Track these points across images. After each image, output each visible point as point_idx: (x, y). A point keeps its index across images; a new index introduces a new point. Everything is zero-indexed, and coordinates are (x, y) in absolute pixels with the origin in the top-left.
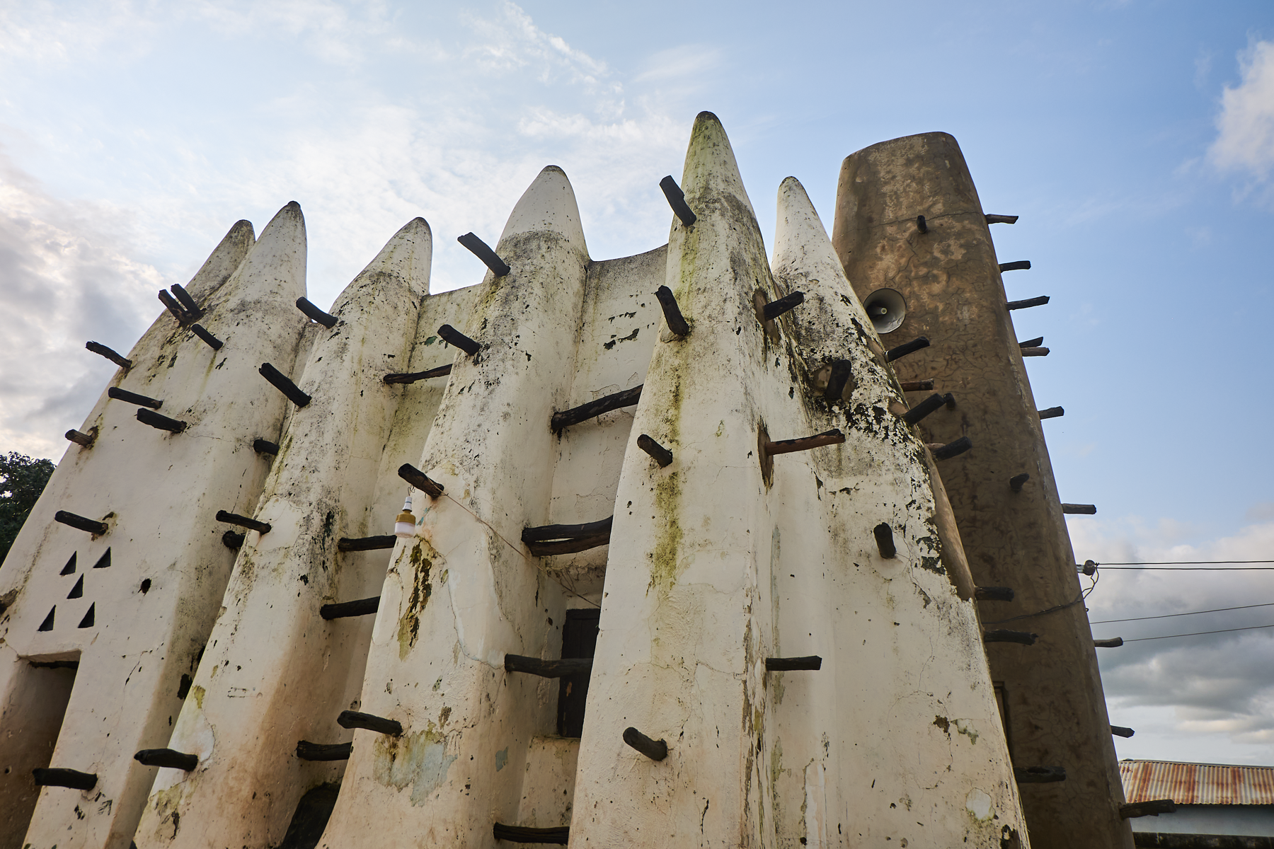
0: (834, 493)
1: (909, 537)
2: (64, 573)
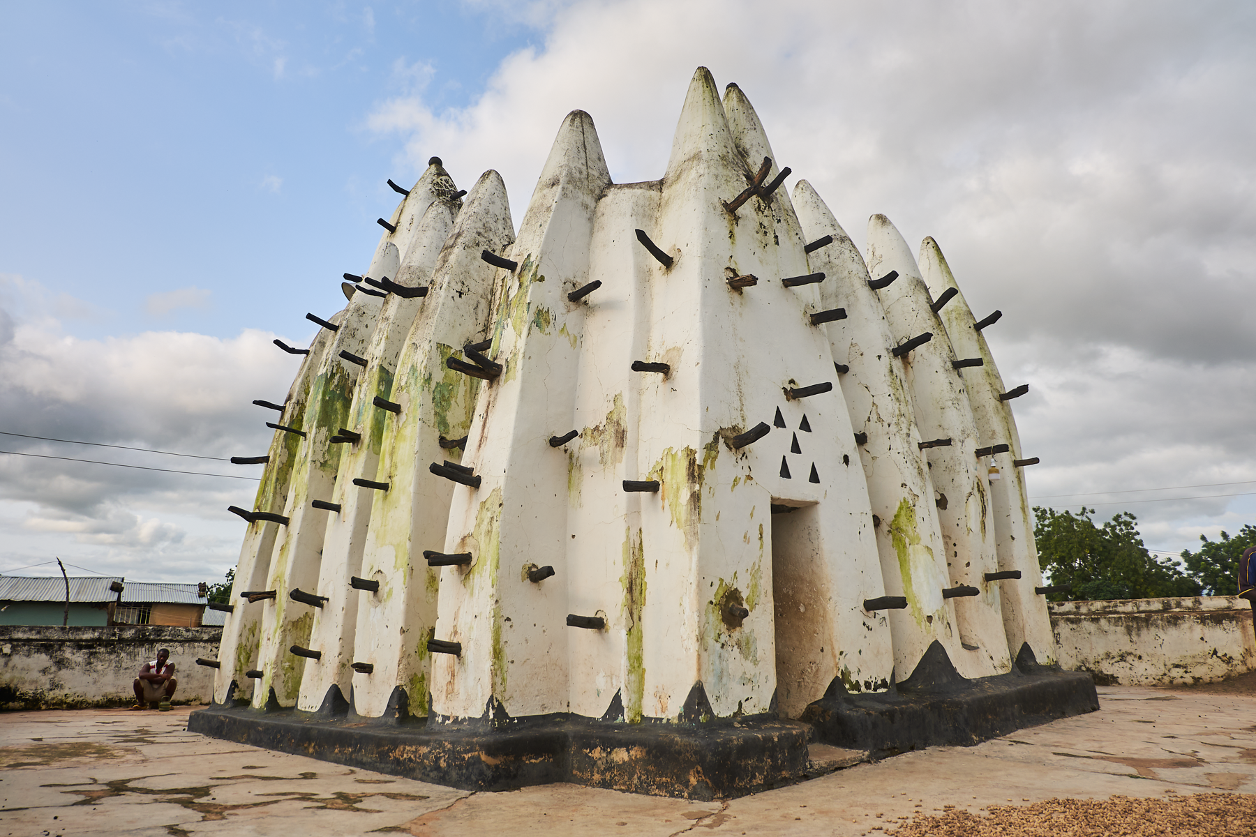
2: (427, 555)
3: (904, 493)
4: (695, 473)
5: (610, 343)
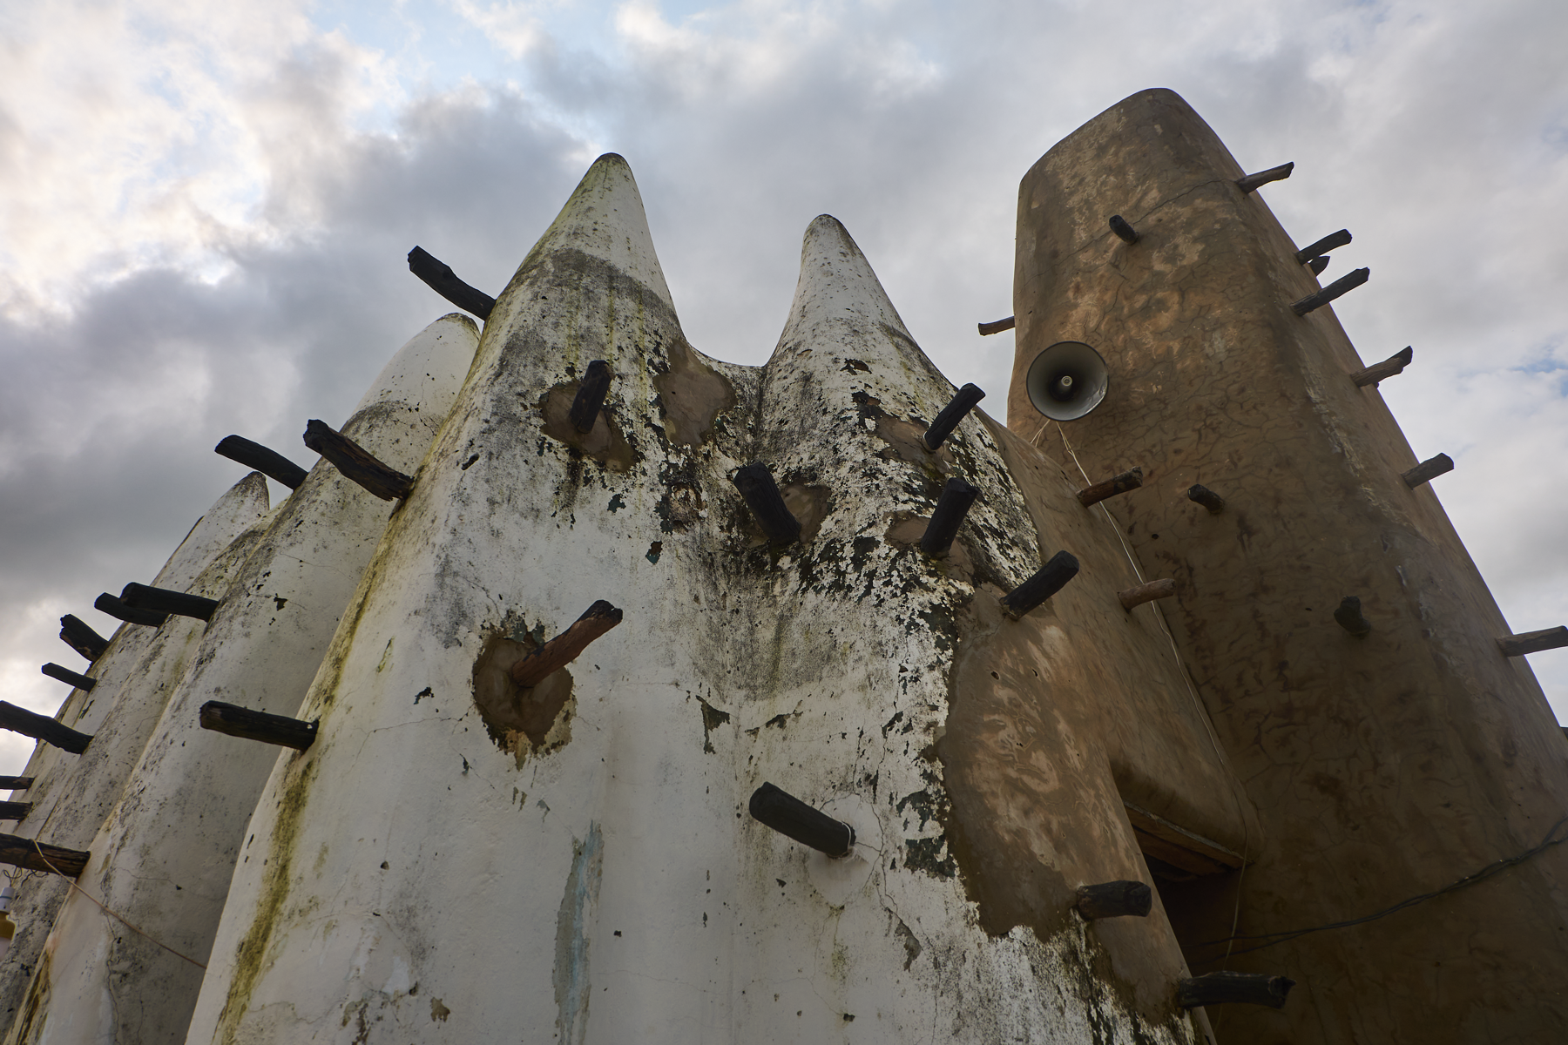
0: (755, 732)
1: (883, 798)
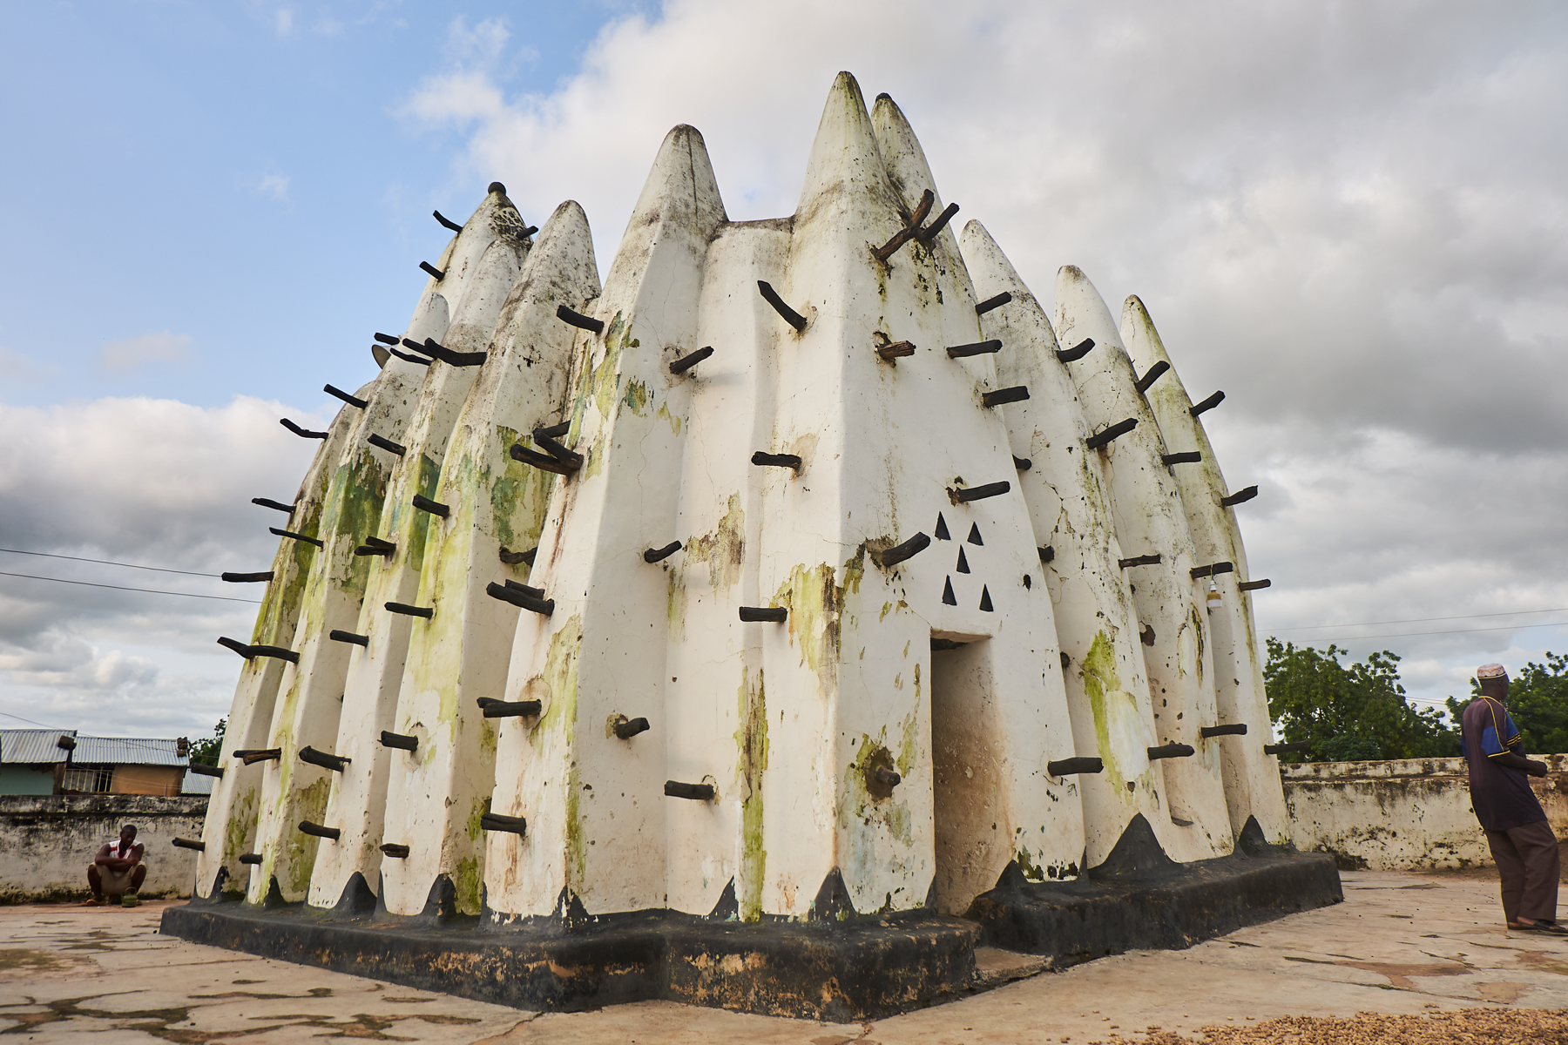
3: (1101, 625)
4: (833, 598)
5: (723, 428)
